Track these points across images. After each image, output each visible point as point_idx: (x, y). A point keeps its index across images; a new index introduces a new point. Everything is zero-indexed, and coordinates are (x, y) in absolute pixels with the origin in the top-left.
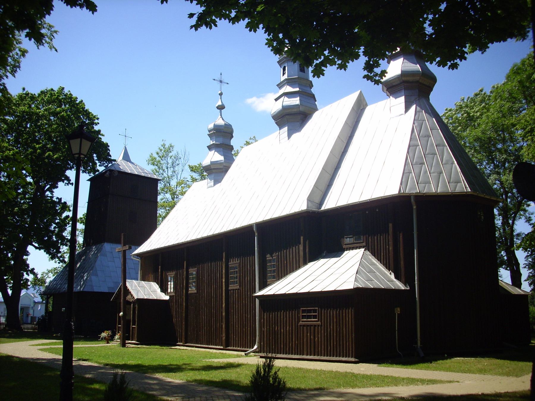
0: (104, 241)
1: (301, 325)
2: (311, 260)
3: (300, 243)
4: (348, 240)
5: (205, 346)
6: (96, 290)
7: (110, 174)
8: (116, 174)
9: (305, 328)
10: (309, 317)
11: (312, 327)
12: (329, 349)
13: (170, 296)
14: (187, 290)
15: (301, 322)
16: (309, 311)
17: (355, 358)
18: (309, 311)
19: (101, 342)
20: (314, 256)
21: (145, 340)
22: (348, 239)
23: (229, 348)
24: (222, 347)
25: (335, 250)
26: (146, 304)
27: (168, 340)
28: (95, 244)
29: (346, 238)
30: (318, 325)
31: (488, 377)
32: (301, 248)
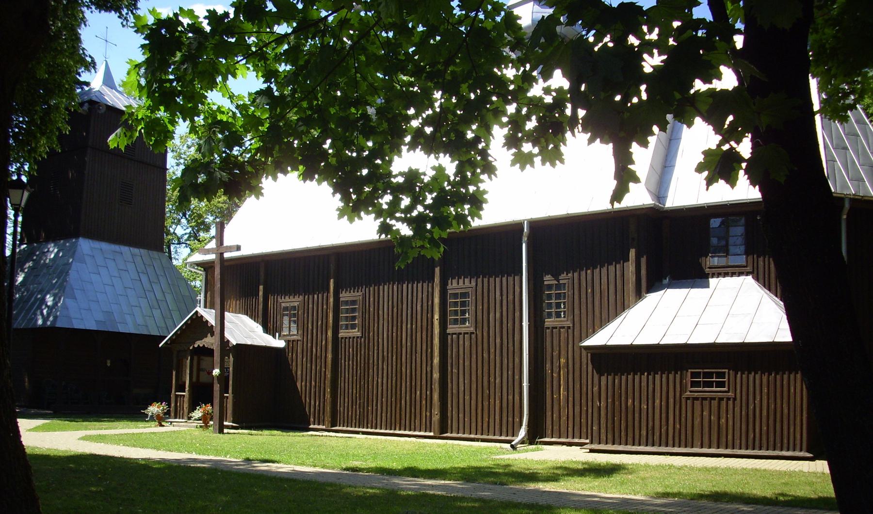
0: (77, 236)
1: (688, 399)
2: (651, 289)
3: (627, 259)
4: (715, 261)
5: (345, 428)
6: (77, 325)
7: (89, 109)
8: (103, 110)
9: (706, 403)
10: (709, 384)
11: (715, 403)
12: (751, 436)
13: (288, 342)
14: (336, 332)
15: (688, 393)
16: (710, 375)
17: (808, 451)
18: (710, 375)
19: (147, 424)
20: (654, 282)
21: (251, 418)
22: (716, 259)
23: (448, 435)
24: (432, 434)
25: (693, 275)
26: (246, 353)
27: (292, 418)
28: (53, 237)
29: (712, 257)
30: (728, 399)
31: (588, 479)
32: (631, 267)
